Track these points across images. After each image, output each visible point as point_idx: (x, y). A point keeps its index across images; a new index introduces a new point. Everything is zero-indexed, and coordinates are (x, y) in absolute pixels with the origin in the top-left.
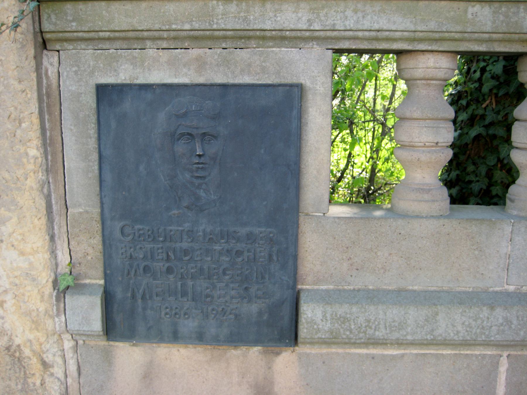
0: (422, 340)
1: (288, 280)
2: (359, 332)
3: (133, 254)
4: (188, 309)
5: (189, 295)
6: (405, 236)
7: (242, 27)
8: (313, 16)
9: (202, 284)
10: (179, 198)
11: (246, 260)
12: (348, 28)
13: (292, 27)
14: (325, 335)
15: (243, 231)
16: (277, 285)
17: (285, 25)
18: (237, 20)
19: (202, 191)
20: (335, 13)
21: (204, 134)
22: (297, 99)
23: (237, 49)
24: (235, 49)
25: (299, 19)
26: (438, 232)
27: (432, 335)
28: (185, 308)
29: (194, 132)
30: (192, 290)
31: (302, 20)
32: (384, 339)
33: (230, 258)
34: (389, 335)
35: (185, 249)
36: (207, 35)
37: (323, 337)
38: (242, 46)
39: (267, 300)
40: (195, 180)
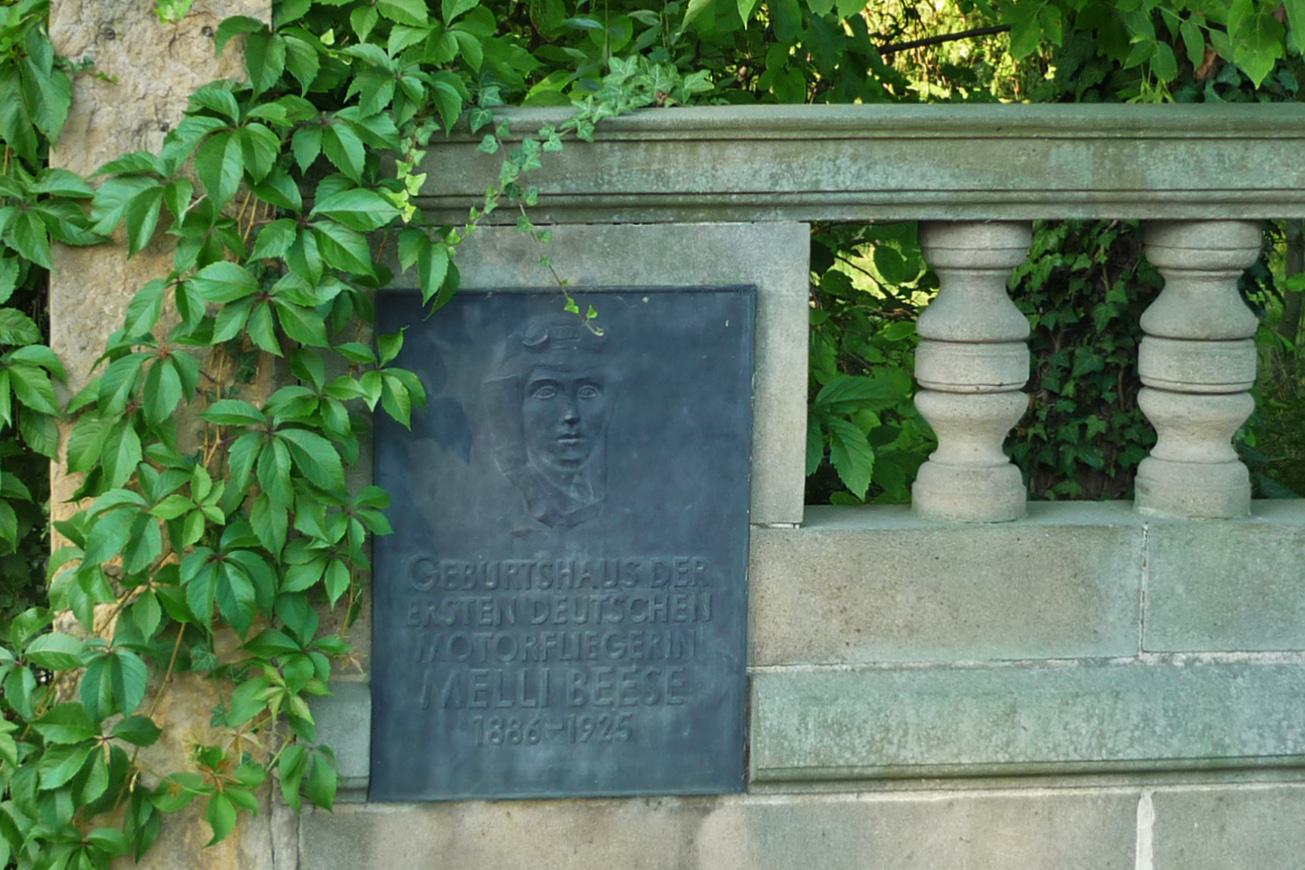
0: (988, 763)
2: (869, 752)
3: (433, 616)
4: (537, 723)
6: (946, 561)
7: (654, 189)
9: (567, 674)
10: (529, 503)
11: (652, 618)
12: (842, 187)
13: (744, 187)
14: (805, 761)
15: (648, 562)
17: (730, 185)
18: (645, 176)
19: (572, 488)
21: (580, 382)
25: (756, 172)
26: (1008, 552)
27: (1006, 752)
28: (532, 721)
32: (916, 765)
34: (926, 755)
35: (536, 603)
37: (802, 764)
38: (650, 219)
40: (559, 468)
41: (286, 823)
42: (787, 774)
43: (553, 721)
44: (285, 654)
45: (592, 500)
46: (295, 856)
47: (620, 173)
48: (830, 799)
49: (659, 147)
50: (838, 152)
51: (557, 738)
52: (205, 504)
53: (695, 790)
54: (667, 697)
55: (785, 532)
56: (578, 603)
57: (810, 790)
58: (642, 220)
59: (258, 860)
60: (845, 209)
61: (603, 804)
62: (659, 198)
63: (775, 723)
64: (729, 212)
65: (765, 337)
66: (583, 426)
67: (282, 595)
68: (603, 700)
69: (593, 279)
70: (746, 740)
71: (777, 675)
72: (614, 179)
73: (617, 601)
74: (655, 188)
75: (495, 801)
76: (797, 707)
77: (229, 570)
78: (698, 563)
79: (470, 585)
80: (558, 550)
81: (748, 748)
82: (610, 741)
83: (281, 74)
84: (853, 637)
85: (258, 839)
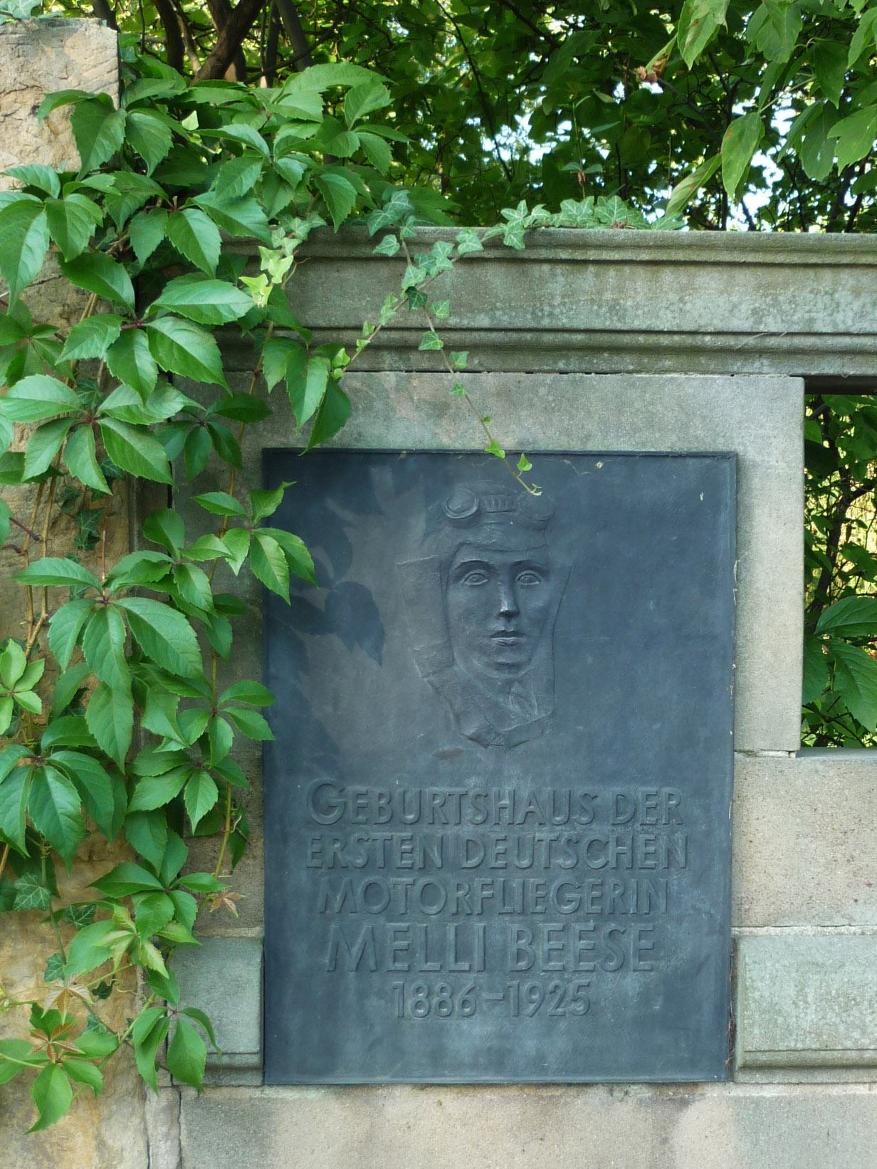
1: (713, 912)
3: (339, 855)
5: (476, 955)
7: (607, 324)
8: (765, 302)
9: (506, 930)
12: (842, 328)
13: (719, 325)
14: (803, 1041)
15: (607, 794)
16: (685, 924)
17: (702, 322)
18: (595, 307)
19: (511, 698)
20: (812, 296)
21: (519, 566)
22: (729, 487)
23: (590, 373)
24: (586, 373)
25: (735, 306)
29: (495, 559)
30: (482, 942)
31: (739, 310)
33: (575, 861)
36: (526, 340)
37: (800, 1046)
38: (604, 367)
39: (662, 963)
40: (495, 674)
41: (164, 1110)
42: (781, 1058)
43: (490, 989)
44: (141, 892)
45: (536, 714)
46: (177, 1149)
47: (564, 304)
48: (835, 1091)
49: (612, 272)
50: (836, 283)
51: (497, 1010)
52: (18, 688)
53: (669, 1076)
54: (633, 962)
55: (778, 761)
56: (520, 843)
57: (810, 1079)
58: (595, 368)
59: (126, 1154)
60: (847, 359)
61: (557, 1092)
62: (613, 337)
63: (767, 994)
64: (703, 360)
65: (749, 517)
66: (524, 622)
67: (129, 817)
68: (554, 964)
69: (535, 442)
70: (732, 1015)
71: (769, 937)
72: (557, 311)
73: (569, 841)
74: (608, 323)
75: (424, 1087)
76: (794, 975)
77: (50, 775)
78: (670, 796)
79: (383, 819)
80: (496, 776)
81: (734, 1026)
82: (563, 1015)
83: (119, 148)
84: (863, 892)
85: (126, 1128)
